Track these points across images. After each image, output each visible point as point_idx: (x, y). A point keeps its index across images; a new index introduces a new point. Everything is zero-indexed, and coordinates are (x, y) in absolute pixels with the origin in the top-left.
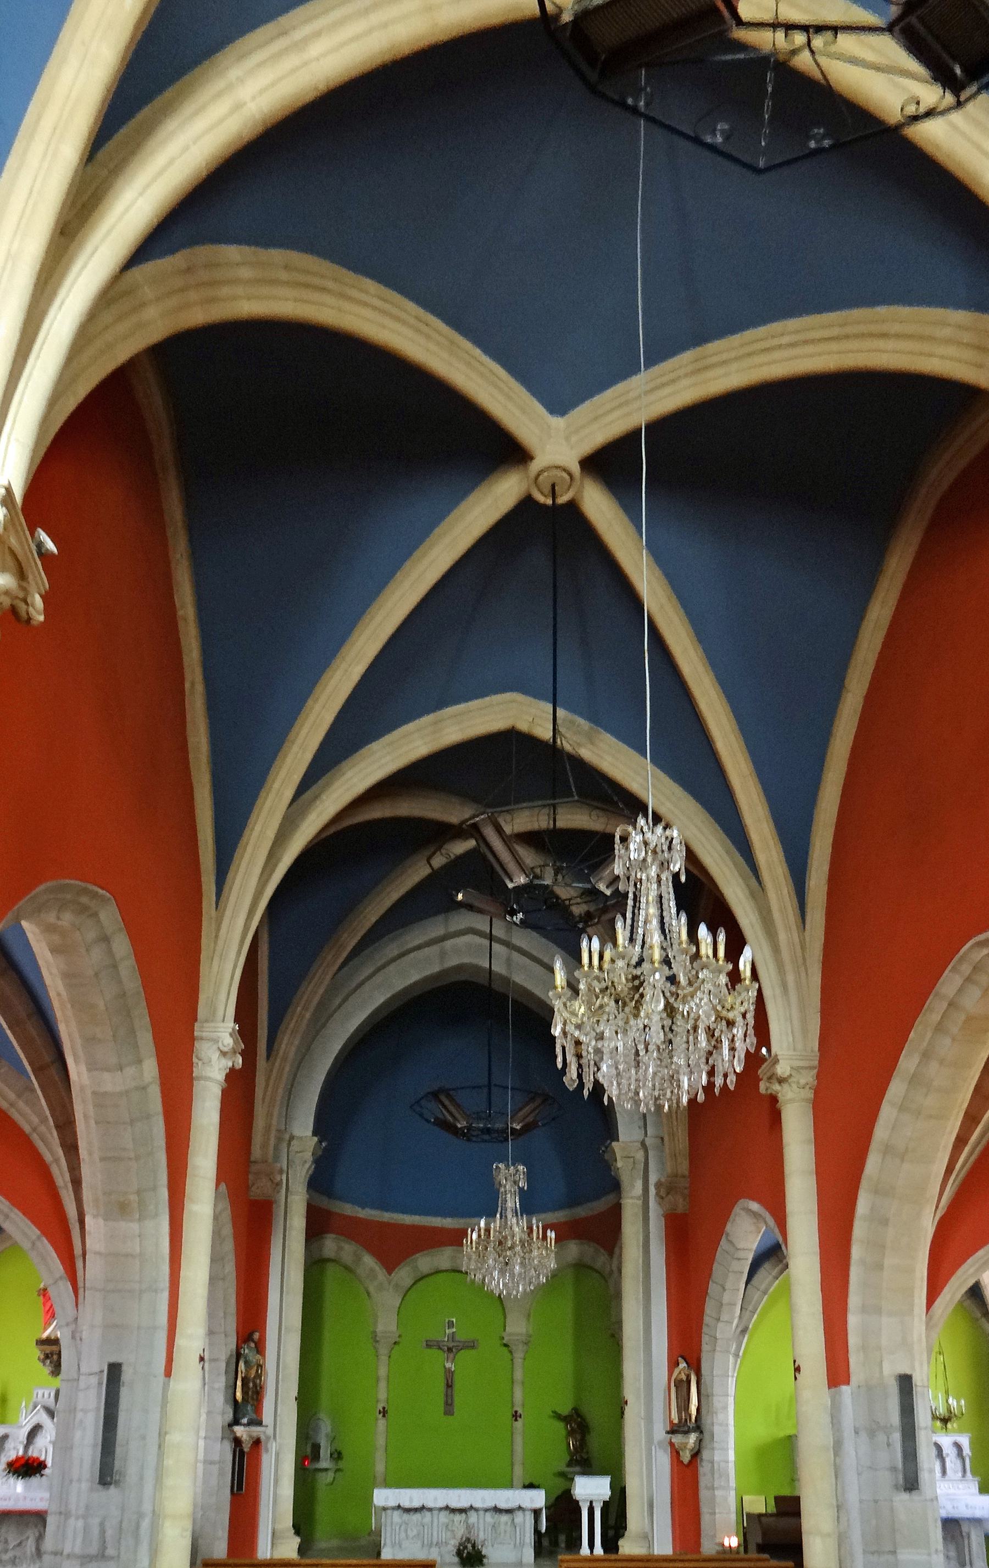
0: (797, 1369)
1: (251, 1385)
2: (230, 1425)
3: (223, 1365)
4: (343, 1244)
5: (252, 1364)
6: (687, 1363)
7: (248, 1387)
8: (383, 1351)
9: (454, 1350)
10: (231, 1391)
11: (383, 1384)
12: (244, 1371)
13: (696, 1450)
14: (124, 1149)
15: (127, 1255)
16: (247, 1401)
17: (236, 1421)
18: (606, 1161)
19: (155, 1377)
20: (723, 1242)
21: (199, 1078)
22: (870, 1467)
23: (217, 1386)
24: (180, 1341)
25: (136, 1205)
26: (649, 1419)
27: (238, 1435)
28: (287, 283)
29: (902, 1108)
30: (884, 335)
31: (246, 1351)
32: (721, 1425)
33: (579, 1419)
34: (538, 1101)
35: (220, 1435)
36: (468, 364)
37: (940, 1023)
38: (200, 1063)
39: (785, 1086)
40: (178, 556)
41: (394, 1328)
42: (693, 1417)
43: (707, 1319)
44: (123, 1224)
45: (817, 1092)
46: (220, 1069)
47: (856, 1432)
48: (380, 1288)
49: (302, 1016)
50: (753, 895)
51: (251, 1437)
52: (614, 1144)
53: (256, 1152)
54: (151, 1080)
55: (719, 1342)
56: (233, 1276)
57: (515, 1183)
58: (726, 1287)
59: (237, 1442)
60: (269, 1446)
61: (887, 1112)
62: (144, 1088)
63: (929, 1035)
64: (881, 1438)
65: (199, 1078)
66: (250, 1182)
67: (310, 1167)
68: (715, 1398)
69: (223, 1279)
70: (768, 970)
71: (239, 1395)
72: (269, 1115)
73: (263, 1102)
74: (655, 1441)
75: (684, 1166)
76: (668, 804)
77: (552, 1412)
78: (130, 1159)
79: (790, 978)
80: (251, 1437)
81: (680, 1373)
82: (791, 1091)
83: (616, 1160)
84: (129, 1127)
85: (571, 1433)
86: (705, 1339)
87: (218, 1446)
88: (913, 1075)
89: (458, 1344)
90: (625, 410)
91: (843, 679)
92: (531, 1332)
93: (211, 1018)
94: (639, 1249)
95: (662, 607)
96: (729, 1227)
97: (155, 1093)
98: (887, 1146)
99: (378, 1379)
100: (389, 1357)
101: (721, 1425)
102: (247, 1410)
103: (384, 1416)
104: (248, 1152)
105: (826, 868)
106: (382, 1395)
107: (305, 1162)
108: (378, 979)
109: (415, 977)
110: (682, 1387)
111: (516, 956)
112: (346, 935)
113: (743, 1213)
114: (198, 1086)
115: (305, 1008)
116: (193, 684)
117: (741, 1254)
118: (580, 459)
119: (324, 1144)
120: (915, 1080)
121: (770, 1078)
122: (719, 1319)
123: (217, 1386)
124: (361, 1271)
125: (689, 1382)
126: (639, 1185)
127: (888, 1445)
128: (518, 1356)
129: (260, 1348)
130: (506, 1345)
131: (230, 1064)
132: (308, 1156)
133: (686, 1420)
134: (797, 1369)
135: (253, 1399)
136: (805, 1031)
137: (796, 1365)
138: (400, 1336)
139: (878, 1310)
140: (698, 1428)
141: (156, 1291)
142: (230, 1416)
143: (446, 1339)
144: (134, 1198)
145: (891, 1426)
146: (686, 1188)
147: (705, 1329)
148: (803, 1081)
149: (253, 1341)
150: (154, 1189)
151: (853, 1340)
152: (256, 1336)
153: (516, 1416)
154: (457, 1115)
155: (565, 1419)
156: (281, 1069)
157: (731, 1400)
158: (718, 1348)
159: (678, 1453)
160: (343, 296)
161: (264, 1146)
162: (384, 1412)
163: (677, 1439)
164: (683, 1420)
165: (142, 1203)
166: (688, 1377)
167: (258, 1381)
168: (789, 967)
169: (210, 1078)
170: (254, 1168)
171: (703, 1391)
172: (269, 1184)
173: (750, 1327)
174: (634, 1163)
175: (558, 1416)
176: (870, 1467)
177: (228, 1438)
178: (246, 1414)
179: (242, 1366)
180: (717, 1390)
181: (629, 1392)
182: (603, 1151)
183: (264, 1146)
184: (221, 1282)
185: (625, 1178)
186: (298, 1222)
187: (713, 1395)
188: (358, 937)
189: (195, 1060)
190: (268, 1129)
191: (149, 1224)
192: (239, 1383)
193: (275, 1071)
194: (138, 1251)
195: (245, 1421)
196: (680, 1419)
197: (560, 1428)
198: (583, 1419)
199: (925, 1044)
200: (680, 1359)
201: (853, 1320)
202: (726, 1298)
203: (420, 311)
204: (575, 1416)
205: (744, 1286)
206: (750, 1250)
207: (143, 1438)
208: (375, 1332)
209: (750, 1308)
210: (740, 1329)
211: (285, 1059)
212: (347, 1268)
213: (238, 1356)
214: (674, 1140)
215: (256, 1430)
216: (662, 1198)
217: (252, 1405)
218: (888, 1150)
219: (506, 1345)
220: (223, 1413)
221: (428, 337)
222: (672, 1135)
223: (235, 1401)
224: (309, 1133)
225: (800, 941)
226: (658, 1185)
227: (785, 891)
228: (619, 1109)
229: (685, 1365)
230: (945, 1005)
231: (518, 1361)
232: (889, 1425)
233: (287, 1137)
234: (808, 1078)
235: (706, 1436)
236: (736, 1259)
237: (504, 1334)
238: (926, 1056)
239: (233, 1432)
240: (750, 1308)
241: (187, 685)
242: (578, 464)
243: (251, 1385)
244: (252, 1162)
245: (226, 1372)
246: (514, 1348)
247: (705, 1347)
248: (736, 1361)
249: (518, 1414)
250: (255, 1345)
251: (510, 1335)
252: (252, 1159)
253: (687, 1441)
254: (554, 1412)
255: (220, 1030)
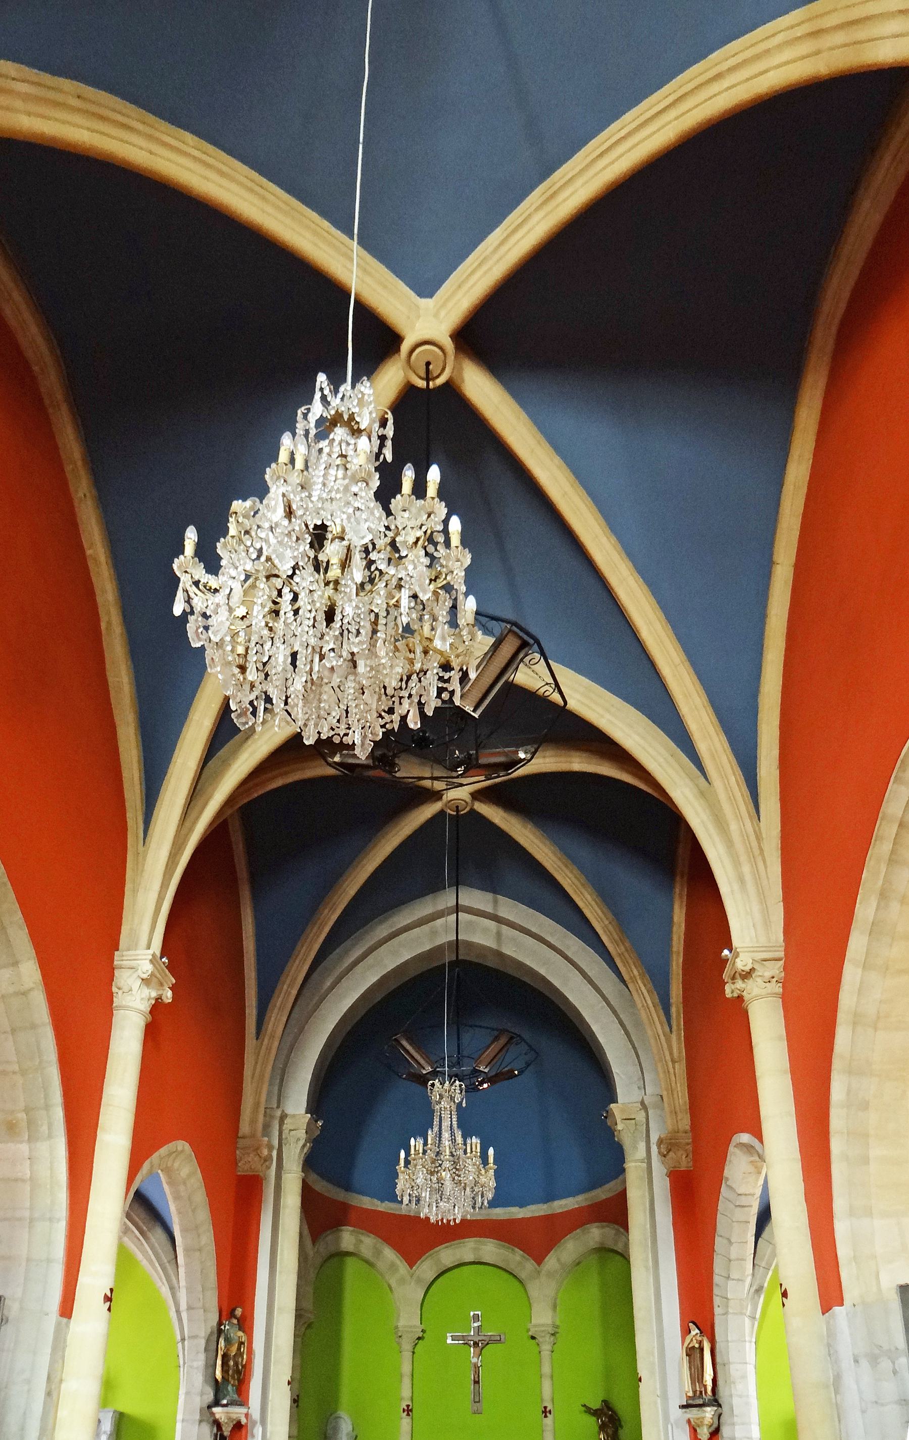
0: (785, 1294)
1: (231, 1363)
2: (209, 1407)
3: (202, 1343)
4: (363, 1238)
5: (234, 1341)
6: (699, 1329)
7: (228, 1366)
8: (407, 1346)
9: (480, 1345)
10: (210, 1370)
11: (407, 1381)
12: (223, 1348)
13: (715, 1425)
14: (8, 1062)
15: (16, 1180)
16: (228, 1381)
17: (216, 1403)
18: (609, 1128)
19: (47, 1314)
20: (723, 1189)
21: (120, 1007)
22: (876, 1402)
23: (195, 1364)
24: (83, 1279)
25: (24, 1124)
26: (664, 1396)
27: (217, 1416)
28: (79, 110)
29: (866, 966)
30: (718, 77)
31: (227, 1327)
32: (740, 1396)
33: (610, 1413)
34: (503, 1041)
35: (198, 1417)
36: (315, 233)
37: (893, 852)
38: (120, 992)
39: (750, 982)
40: (81, 494)
41: (417, 1322)
42: (709, 1388)
43: (717, 1279)
44: (11, 1145)
45: (785, 983)
46: (142, 999)
47: (856, 1361)
48: (402, 1281)
49: (288, 993)
50: (702, 794)
51: (229, 1419)
52: (612, 1106)
53: (245, 1128)
54: (32, 985)
55: (731, 1303)
56: (211, 1248)
57: (452, 1099)
58: (733, 1240)
59: (217, 1424)
60: (255, 1431)
61: (851, 974)
62: (24, 994)
63: (883, 868)
64: (885, 1364)
65: (120, 1007)
66: (238, 1157)
67: (304, 1146)
68: (732, 1367)
69: (200, 1250)
70: (724, 867)
71: (219, 1375)
72: (258, 1092)
73: (253, 1078)
74: (672, 1420)
75: (685, 1122)
76: (608, 716)
77: (582, 1406)
78: (14, 1073)
79: (746, 869)
80: (229, 1419)
81: (692, 1340)
82: (757, 986)
83: (616, 1124)
84: (11, 1037)
85: (602, 1428)
86: (717, 1301)
87: (195, 1428)
88: (873, 923)
89: (484, 1338)
90: (485, 268)
91: (771, 555)
92: (558, 1323)
93: (134, 946)
94: (645, 1212)
95: (565, 494)
96: (726, 1173)
97: (39, 1001)
98: (856, 1015)
99: (402, 1376)
100: (413, 1353)
101: (740, 1396)
102: (227, 1390)
103: (408, 1415)
104: (237, 1129)
105: (776, 752)
106: (406, 1392)
107: (298, 1139)
108: (370, 960)
109: (406, 955)
110: (694, 1354)
111: (505, 929)
112: (326, 911)
113: (737, 1151)
114: (118, 1016)
115: (291, 986)
116: (109, 623)
117: (743, 1201)
118: (449, 334)
119: (320, 1123)
120: (875, 930)
121: (733, 978)
122: (729, 1277)
123: (195, 1364)
124: (380, 1265)
125: (701, 1349)
126: (642, 1146)
127: (895, 1372)
128: (546, 1348)
129: (245, 1324)
130: (533, 1338)
131: (154, 994)
132: (302, 1134)
133: (701, 1392)
134: (785, 1294)
135: (233, 1378)
136: (767, 923)
137: (783, 1289)
138: (423, 1331)
139: (868, 1212)
140: (715, 1402)
141: (51, 1220)
142: (210, 1396)
143: (472, 1333)
144: (22, 1116)
145: (897, 1349)
146: (688, 1144)
147: (716, 1291)
148: (768, 974)
149: (235, 1318)
150: (47, 1107)
151: (843, 1251)
152: (239, 1311)
153: (546, 1412)
154: (422, 1062)
155: (596, 1413)
156: (269, 1049)
157: (750, 1369)
158: (730, 1310)
159: (695, 1430)
160: (150, 137)
161: (253, 1121)
162: (408, 1411)
163: (693, 1413)
164: (698, 1392)
165: (31, 1123)
166: (700, 1342)
167: (240, 1360)
168: (743, 858)
169: (129, 1007)
170: (241, 1143)
171: (718, 1359)
172: (257, 1158)
173: (766, 1285)
174: (636, 1125)
175: (588, 1410)
176: (876, 1402)
177: (208, 1422)
178: (226, 1396)
179: (222, 1343)
180: (733, 1356)
181: (643, 1370)
182: (606, 1117)
183: (253, 1121)
184: (198, 1254)
185: (626, 1140)
186: (292, 1200)
187: (729, 1363)
188: (338, 912)
189: (114, 989)
190: (257, 1105)
191: (42, 1147)
192: (219, 1362)
193: (264, 1047)
194: (28, 1176)
195: (225, 1402)
196: (695, 1392)
197: (592, 1423)
198: (614, 1412)
199: (880, 883)
200: (691, 1324)
201: (841, 1227)
202: (734, 1252)
203: (255, 175)
204: (605, 1410)
205: (753, 1238)
206: (753, 1195)
207: (28, 1382)
208: (397, 1327)
209: (763, 1264)
210: (754, 1288)
211: (272, 1037)
212: (367, 1262)
213: (220, 1332)
214: (673, 1094)
215: (238, 1412)
216: (665, 1156)
217: (233, 1385)
218: (857, 1020)
219: (533, 1338)
220: (202, 1394)
221: (264, 198)
222: (671, 1091)
223: (216, 1380)
224: (303, 1111)
225: (755, 831)
226: (660, 1142)
227: (733, 779)
228: (617, 1071)
229: (697, 1331)
230: (894, 828)
231: (546, 1354)
232: (893, 1349)
233: (278, 1113)
234: (776, 969)
235: (725, 1409)
236: (739, 1206)
237: (529, 1326)
238: (883, 895)
239: (213, 1414)
240: (763, 1264)
241: (103, 625)
242: (450, 339)
243: (231, 1363)
244: (238, 1137)
245: (206, 1350)
246: (540, 1339)
247: (717, 1311)
248: (753, 1325)
249: (548, 1410)
250: (238, 1321)
251: (535, 1326)
252: (240, 1134)
253: (703, 1415)
254: (584, 1406)
255: (139, 957)
